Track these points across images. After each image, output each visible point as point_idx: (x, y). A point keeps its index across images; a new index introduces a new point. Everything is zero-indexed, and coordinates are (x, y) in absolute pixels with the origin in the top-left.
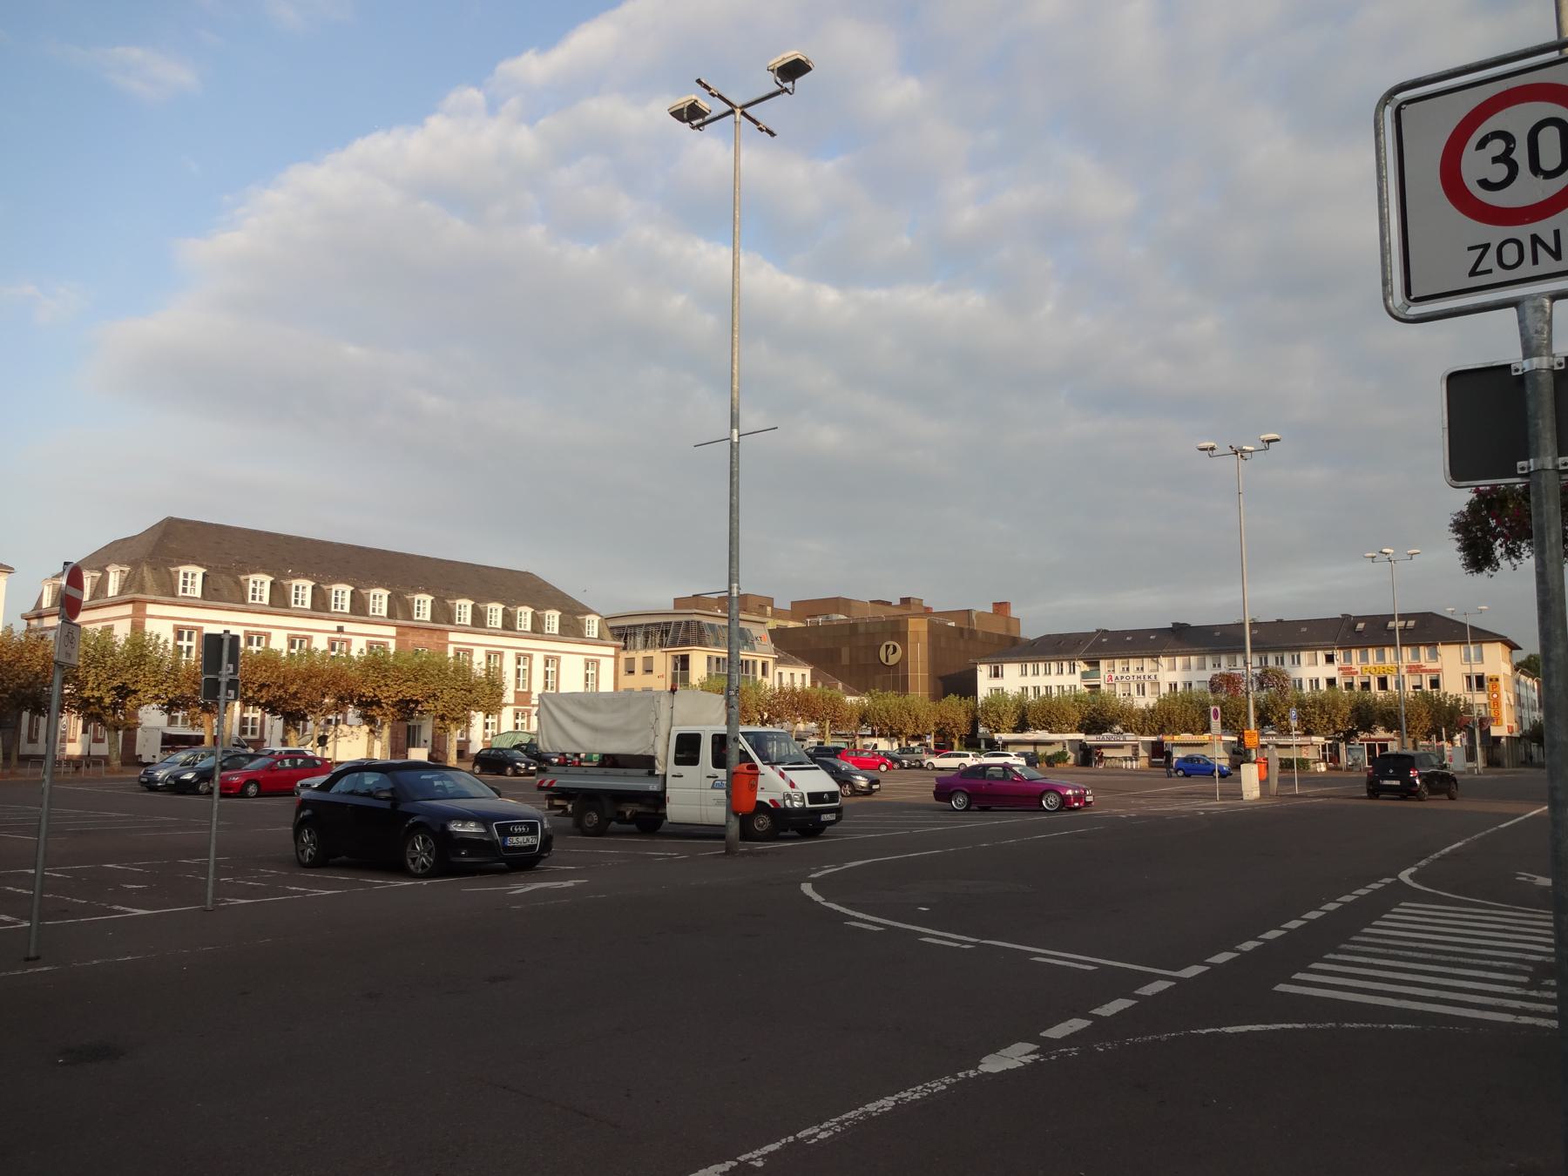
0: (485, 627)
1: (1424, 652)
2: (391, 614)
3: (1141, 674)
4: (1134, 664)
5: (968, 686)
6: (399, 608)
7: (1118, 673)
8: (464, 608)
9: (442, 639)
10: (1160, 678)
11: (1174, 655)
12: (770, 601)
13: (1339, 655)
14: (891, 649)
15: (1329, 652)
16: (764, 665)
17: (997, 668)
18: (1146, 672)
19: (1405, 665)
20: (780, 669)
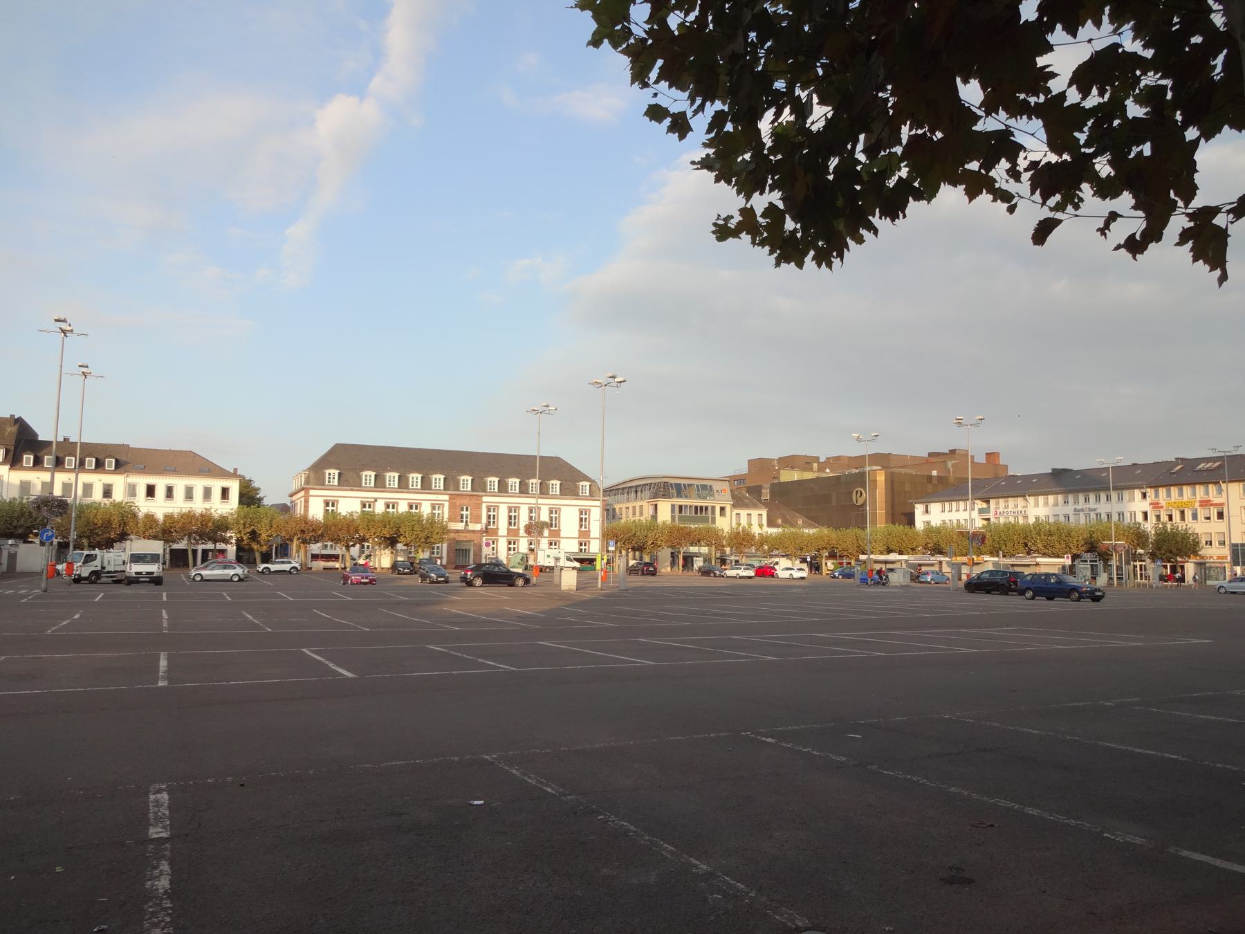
0: (507, 493)
1: (1212, 489)
2: (445, 489)
3: (1016, 510)
4: (1011, 501)
5: (910, 519)
6: (451, 484)
7: (1001, 510)
8: (493, 481)
9: (478, 500)
10: (1028, 513)
11: (1046, 494)
12: (816, 459)
13: (1151, 492)
14: (859, 493)
15: (1143, 491)
16: (722, 509)
17: (927, 507)
18: (1020, 509)
19: (1198, 498)
20: (736, 511)
